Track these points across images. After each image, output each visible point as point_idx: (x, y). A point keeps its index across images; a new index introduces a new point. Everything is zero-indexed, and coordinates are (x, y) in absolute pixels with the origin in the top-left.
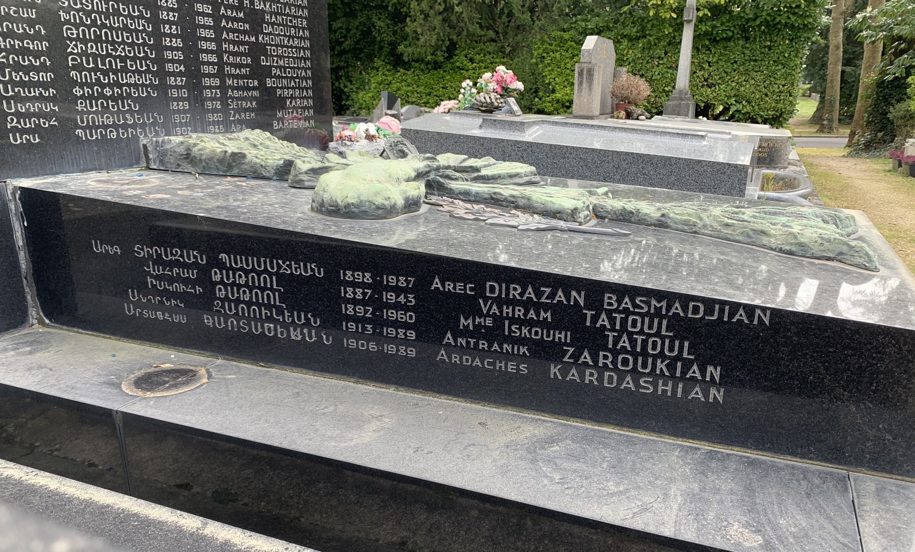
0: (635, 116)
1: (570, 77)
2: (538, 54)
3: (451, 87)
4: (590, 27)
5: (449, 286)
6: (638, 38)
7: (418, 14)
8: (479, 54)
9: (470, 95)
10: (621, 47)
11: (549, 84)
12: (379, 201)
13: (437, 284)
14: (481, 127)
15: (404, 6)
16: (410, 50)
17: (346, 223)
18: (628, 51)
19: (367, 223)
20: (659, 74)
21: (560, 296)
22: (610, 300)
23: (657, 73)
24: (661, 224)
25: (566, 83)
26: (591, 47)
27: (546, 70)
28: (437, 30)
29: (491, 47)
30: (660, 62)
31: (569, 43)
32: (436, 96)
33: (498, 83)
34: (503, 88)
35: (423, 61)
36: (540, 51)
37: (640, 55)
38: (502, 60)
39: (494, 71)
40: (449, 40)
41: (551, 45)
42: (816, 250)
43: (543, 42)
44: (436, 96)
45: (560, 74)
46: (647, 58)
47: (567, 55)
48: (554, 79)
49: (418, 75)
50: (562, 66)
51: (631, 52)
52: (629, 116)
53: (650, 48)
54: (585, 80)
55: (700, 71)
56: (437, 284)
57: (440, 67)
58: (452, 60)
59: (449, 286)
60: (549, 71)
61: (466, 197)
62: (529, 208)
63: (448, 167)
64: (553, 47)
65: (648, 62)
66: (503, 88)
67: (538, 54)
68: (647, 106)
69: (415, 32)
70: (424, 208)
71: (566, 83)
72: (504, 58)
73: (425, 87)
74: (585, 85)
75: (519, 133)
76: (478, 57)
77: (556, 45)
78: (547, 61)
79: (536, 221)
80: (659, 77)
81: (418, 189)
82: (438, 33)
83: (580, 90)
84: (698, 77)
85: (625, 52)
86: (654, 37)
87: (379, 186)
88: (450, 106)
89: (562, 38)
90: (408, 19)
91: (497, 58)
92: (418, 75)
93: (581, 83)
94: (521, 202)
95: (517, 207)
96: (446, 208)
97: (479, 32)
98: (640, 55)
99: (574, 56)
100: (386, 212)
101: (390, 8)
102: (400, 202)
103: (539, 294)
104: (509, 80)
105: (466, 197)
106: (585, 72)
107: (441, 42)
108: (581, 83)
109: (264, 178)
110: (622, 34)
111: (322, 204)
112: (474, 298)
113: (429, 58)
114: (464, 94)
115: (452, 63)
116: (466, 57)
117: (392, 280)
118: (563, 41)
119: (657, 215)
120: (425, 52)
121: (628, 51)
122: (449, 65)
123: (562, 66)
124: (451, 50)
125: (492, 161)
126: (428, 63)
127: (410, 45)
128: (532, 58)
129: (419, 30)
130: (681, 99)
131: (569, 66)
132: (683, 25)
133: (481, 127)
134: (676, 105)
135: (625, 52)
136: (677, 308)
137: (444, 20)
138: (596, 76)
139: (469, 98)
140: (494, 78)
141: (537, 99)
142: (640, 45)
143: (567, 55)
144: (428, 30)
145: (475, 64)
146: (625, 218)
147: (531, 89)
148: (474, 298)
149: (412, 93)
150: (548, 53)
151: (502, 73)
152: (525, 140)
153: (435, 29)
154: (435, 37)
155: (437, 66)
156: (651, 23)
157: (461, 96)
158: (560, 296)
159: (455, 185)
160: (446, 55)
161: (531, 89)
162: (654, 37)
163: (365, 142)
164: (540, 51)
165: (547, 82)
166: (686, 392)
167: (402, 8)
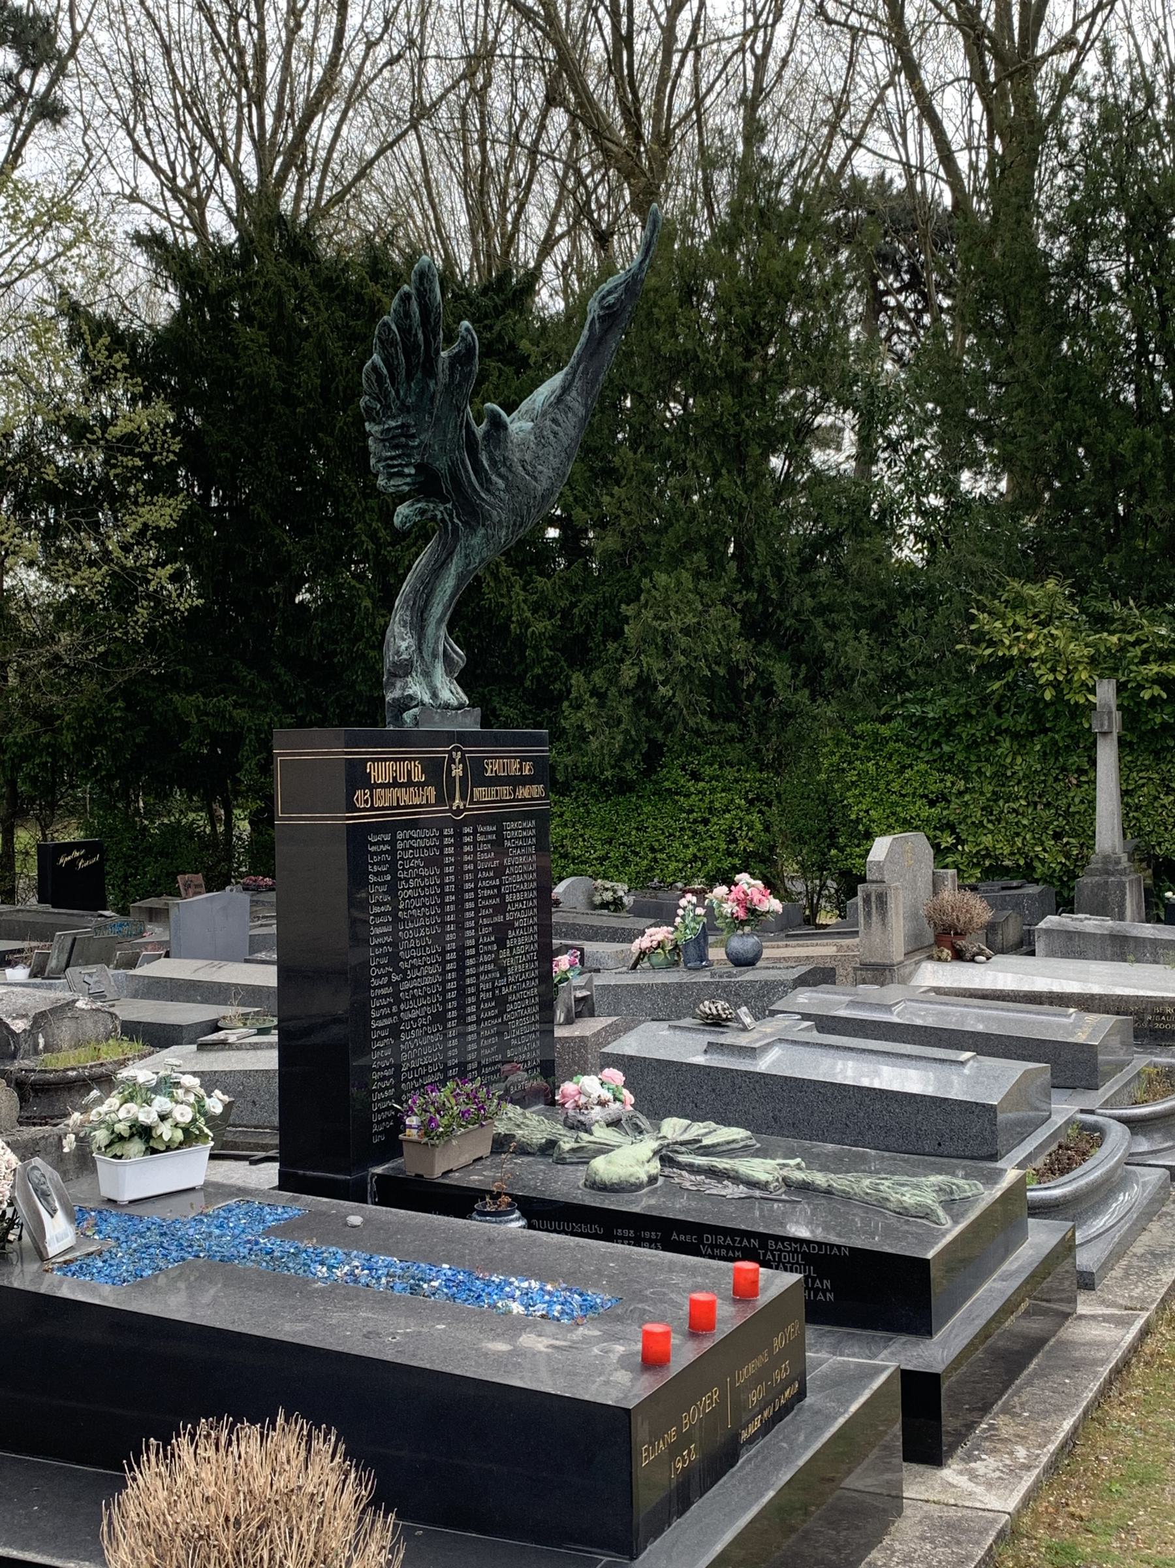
0: (968, 955)
1: (899, 809)
2: (831, 765)
3: (655, 828)
4: (931, 715)
5: (682, 1237)
6: (1032, 734)
7: (587, 697)
8: (711, 765)
9: (694, 920)
10: (999, 752)
11: (858, 821)
12: (633, 1180)
13: (675, 1236)
14: (706, 1052)
15: (556, 679)
16: (568, 760)
17: (614, 1197)
18: (1014, 759)
19: (626, 1196)
20: (1082, 802)
21: (745, 1242)
22: (771, 1243)
23: (1077, 800)
24: (828, 1192)
25: (892, 820)
26: (882, 858)
27: (849, 794)
28: (623, 726)
29: (735, 752)
30: (1083, 779)
31: (891, 745)
32: (624, 844)
33: (739, 902)
34: (748, 909)
35: (595, 779)
36: (835, 759)
37: (1039, 767)
38: (758, 775)
39: (730, 883)
40: (648, 740)
41: (855, 747)
42: (913, 1212)
43: (839, 742)
44: (624, 844)
45: (878, 803)
46: (1054, 772)
47: (890, 767)
48: (867, 811)
49: (584, 805)
50: (882, 786)
51: (1019, 760)
52: (959, 956)
53: (1057, 752)
54: (874, 910)
55: (1167, 794)
56: (675, 1236)
57: (631, 789)
58: (654, 777)
59: (682, 1237)
60: (854, 796)
61: (693, 1169)
62: (737, 1179)
63: (676, 1143)
64: (860, 752)
65: (1056, 780)
66: (748, 909)
67: (831, 765)
68: (1064, 865)
69: (581, 727)
70: (661, 1180)
71: (892, 820)
72: (761, 771)
73: (602, 827)
74: (875, 918)
75: (748, 1061)
76: (708, 771)
77: (866, 748)
78: (851, 776)
79: (741, 1190)
80: (1083, 807)
81: (655, 1167)
82: (627, 732)
83: (868, 924)
84: (1163, 806)
85: (1009, 760)
86: (1063, 733)
87: (632, 1170)
88: (660, 937)
89: (876, 734)
90: (566, 704)
91: (747, 771)
92: (584, 805)
93: (868, 915)
94: (732, 1174)
95: (729, 1178)
96: (677, 1180)
97: (707, 725)
98: (1039, 767)
99: (904, 767)
100: (636, 1187)
101: (528, 683)
102: (645, 1179)
103: (734, 1241)
104: (757, 897)
105: (693, 1169)
106: (873, 899)
107: (631, 746)
108: (868, 915)
109: (529, 1154)
110: (999, 726)
111: (594, 1183)
112: (697, 1245)
113: (608, 774)
114: (683, 917)
115: (656, 782)
116: (683, 769)
117: (647, 1234)
118: (878, 742)
119: (825, 1185)
120: (601, 763)
121: (1014, 759)
122: (650, 786)
123: (882, 786)
124: (653, 756)
125: (713, 1125)
126: (606, 782)
127: (569, 750)
128: (819, 772)
129: (588, 726)
130: (1108, 873)
131: (895, 787)
132: (1094, 744)
133: (706, 1052)
134: (1098, 884)
135: (1009, 760)
136: (805, 1247)
137: (638, 703)
138: (891, 904)
139: (692, 925)
140: (732, 896)
141: (833, 852)
142: (1038, 747)
143: (890, 767)
144: (607, 723)
145: (701, 784)
146: (805, 1188)
147: (820, 831)
148: (697, 1245)
149: (573, 838)
150: (850, 763)
151: (745, 887)
152: (758, 1070)
153: (620, 721)
154: (620, 737)
155: (624, 787)
156: (1053, 708)
157: (678, 920)
158: (745, 1242)
159: (682, 1158)
160: (643, 766)
161: (820, 831)
162: (1063, 733)
163: (598, 1108)
164: (835, 759)
165: (853, 817)
166: (816, 1296)
167: (553, 682)
